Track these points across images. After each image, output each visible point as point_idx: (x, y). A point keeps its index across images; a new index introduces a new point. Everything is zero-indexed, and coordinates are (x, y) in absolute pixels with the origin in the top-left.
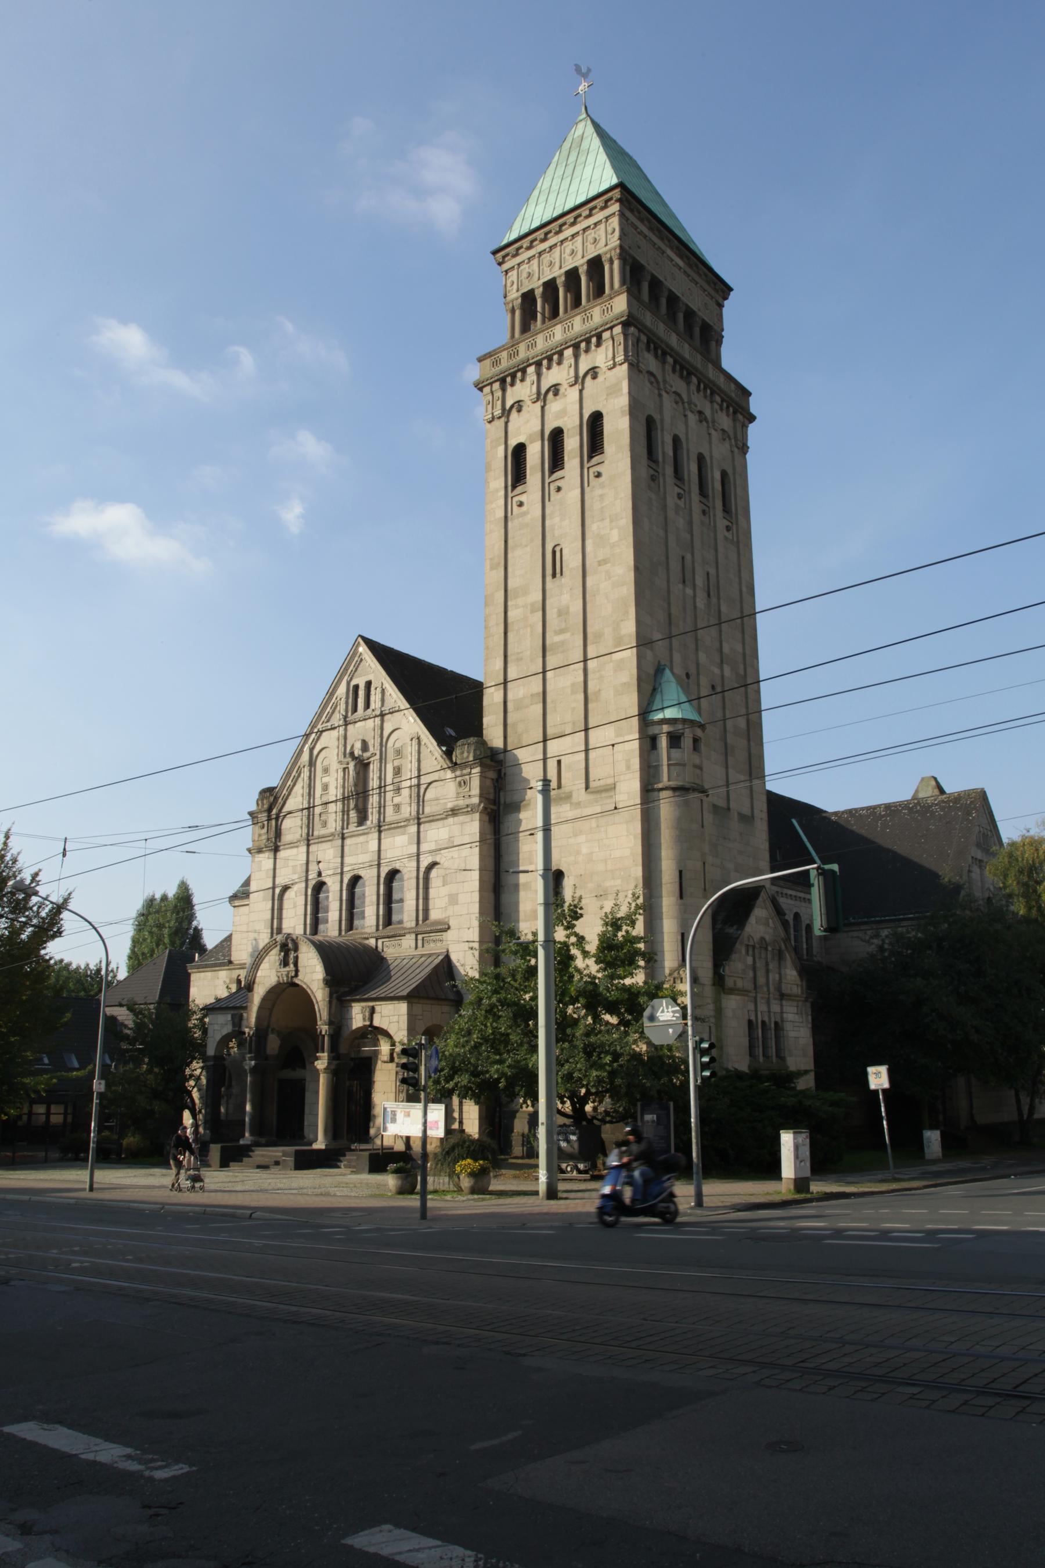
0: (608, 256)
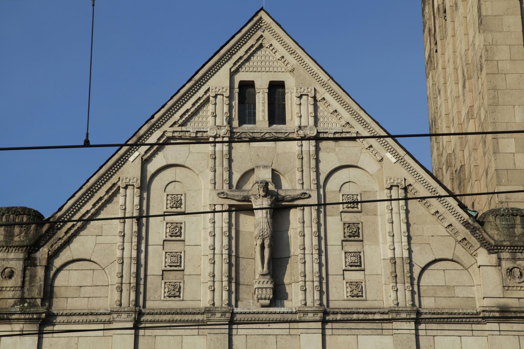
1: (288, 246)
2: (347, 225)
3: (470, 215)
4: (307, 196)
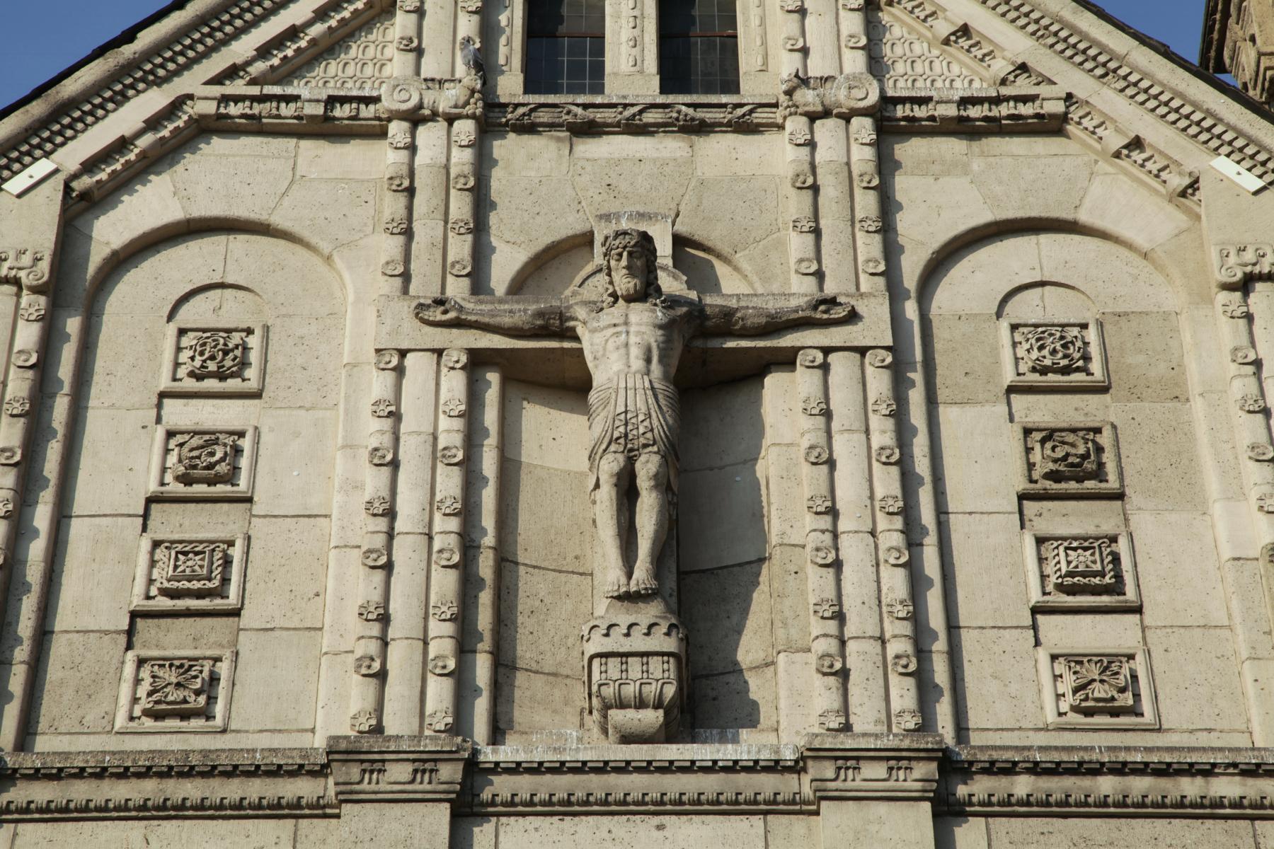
1: (757, 516)
2: (1038, 436)
4: (839, 313)
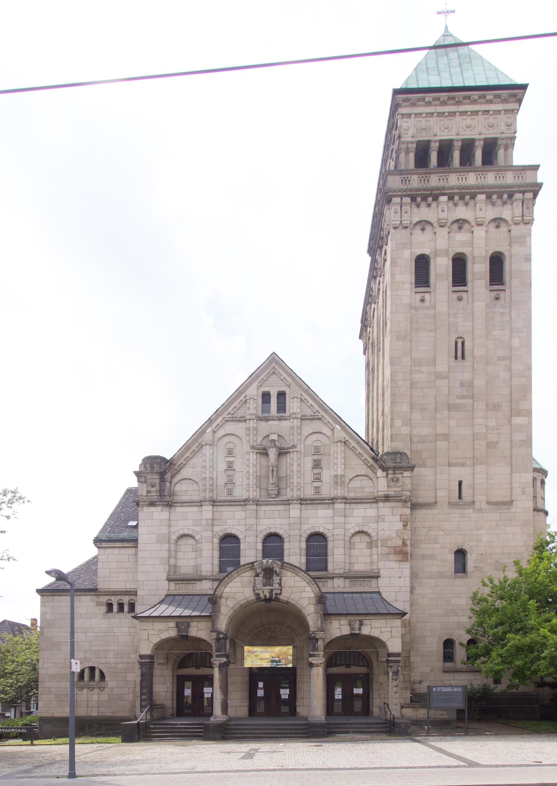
0: (504, 142)
3: (375, 454)
